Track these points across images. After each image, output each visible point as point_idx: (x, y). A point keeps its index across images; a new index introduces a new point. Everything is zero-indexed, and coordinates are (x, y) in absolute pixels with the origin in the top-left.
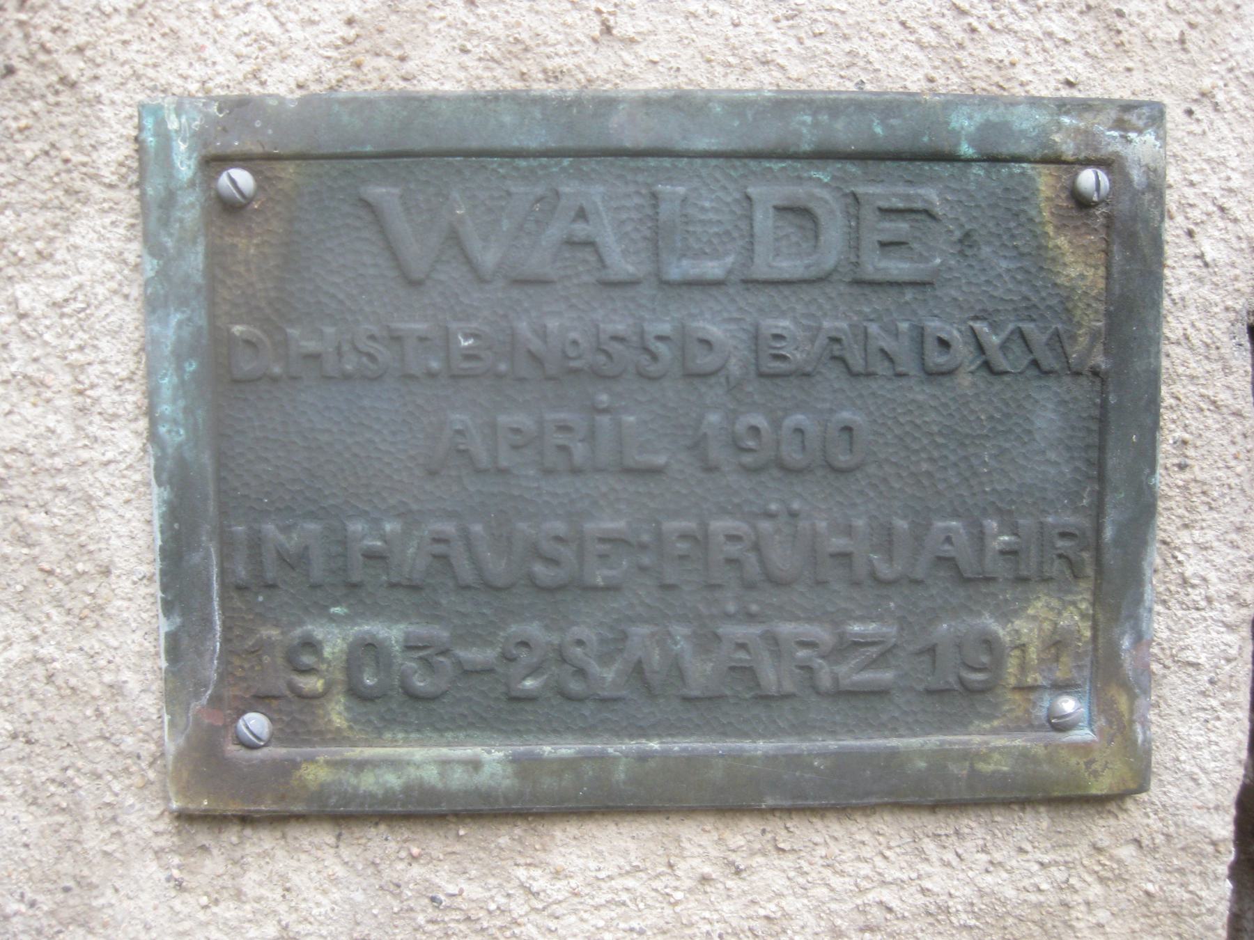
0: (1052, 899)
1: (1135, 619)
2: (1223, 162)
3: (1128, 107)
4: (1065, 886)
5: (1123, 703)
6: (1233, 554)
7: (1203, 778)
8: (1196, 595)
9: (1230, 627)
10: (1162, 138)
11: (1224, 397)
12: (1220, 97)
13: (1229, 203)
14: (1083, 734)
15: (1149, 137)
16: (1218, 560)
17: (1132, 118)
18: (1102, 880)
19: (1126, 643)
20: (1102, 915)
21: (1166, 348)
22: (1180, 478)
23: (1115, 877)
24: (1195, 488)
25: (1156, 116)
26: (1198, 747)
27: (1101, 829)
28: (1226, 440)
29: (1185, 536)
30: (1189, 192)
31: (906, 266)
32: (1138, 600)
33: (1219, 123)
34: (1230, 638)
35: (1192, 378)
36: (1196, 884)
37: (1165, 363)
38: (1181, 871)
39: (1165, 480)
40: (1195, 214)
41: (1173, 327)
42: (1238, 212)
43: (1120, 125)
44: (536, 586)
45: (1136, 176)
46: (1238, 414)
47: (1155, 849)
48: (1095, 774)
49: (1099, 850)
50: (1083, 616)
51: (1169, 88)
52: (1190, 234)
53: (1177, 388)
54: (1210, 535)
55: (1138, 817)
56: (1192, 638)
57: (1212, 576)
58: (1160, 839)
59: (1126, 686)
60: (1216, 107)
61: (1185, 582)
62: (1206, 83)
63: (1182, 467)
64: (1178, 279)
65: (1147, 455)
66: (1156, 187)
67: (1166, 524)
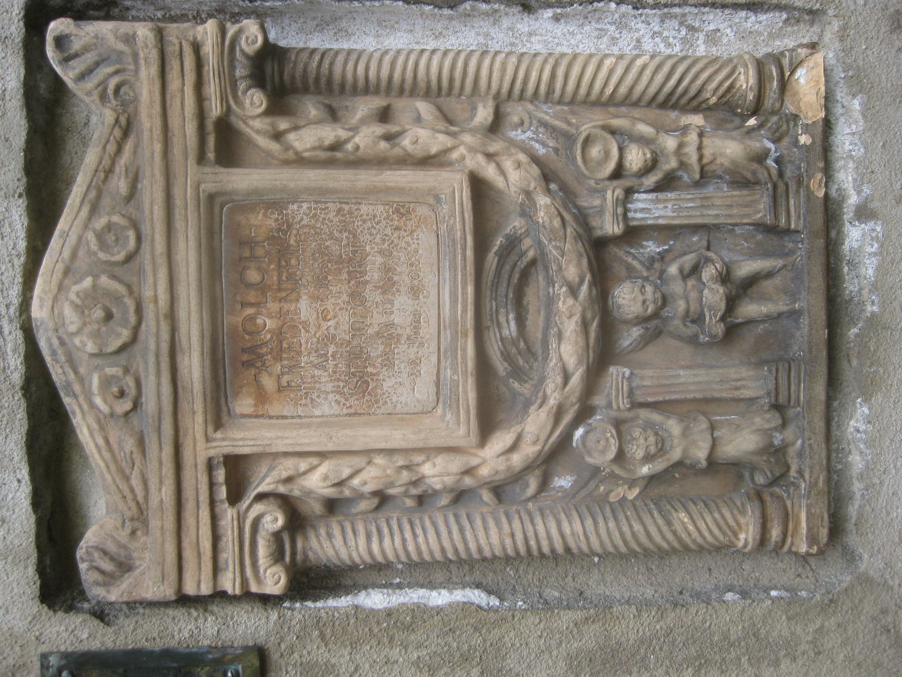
0: (299, 669)
1: (203, 654)
2: (58, 632)
3: (42, 666)
4: (295, 665)
5: (229, 657)
6: (182, 621)
7: (257, 624)
8: (196, 632)
9: (206, 620)
10: (51, 653)
11: (131, 627)
12: (37, 634)
13: (70, 629)
14: (240, 668)
15: (51, 659)
16: (184, 626)
17: (45, 664)
18: (293, 653)
19: (210, 656)
20: (305, 652)
21: (117, 648)
22: (158, 640)
23: (291, 649)
24: (161, 635)
25: (44, 657)
26: (246, 627)
27: (275, 656)
28: (145, 626)
29: (177, 637)
30: (68, 642)
31: (196, 374)
32: (196, 653)
33: (45, 633)
34: (209, 620)
35: (126, 638)
36: (294, 623)
37: (122, 647)
38: (289, 628)
39: (157, 646)
40: (74, 640)
41: (110, 645)
42: (73, 626)
43: (48, 668)
44: (775, 318)
45: (63, 662)
46: (137, 622)
47: (282, 637)
48: (252, 665)
49: (282, 655)
50: (202, 669)
51: (36, 649)
52: (81, 641)
53: (130, 642)
54: (176, 629)
55: (271, 645)
56: (209, 633)
57: (189, 627)
58: (278, 636)
59: (224, 656)
60: (41, 634)
61: (192, 636)
62: (33, 638)
63: (154, 639)
64: (95, 645)
65: (150, 654)
66: (66, 655)
67: (172, 644)
